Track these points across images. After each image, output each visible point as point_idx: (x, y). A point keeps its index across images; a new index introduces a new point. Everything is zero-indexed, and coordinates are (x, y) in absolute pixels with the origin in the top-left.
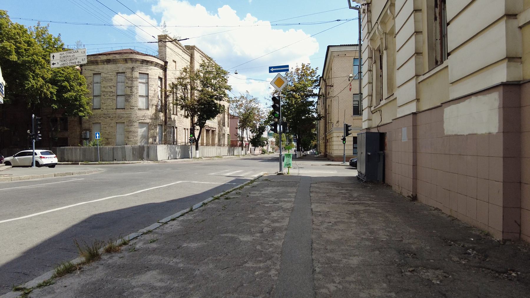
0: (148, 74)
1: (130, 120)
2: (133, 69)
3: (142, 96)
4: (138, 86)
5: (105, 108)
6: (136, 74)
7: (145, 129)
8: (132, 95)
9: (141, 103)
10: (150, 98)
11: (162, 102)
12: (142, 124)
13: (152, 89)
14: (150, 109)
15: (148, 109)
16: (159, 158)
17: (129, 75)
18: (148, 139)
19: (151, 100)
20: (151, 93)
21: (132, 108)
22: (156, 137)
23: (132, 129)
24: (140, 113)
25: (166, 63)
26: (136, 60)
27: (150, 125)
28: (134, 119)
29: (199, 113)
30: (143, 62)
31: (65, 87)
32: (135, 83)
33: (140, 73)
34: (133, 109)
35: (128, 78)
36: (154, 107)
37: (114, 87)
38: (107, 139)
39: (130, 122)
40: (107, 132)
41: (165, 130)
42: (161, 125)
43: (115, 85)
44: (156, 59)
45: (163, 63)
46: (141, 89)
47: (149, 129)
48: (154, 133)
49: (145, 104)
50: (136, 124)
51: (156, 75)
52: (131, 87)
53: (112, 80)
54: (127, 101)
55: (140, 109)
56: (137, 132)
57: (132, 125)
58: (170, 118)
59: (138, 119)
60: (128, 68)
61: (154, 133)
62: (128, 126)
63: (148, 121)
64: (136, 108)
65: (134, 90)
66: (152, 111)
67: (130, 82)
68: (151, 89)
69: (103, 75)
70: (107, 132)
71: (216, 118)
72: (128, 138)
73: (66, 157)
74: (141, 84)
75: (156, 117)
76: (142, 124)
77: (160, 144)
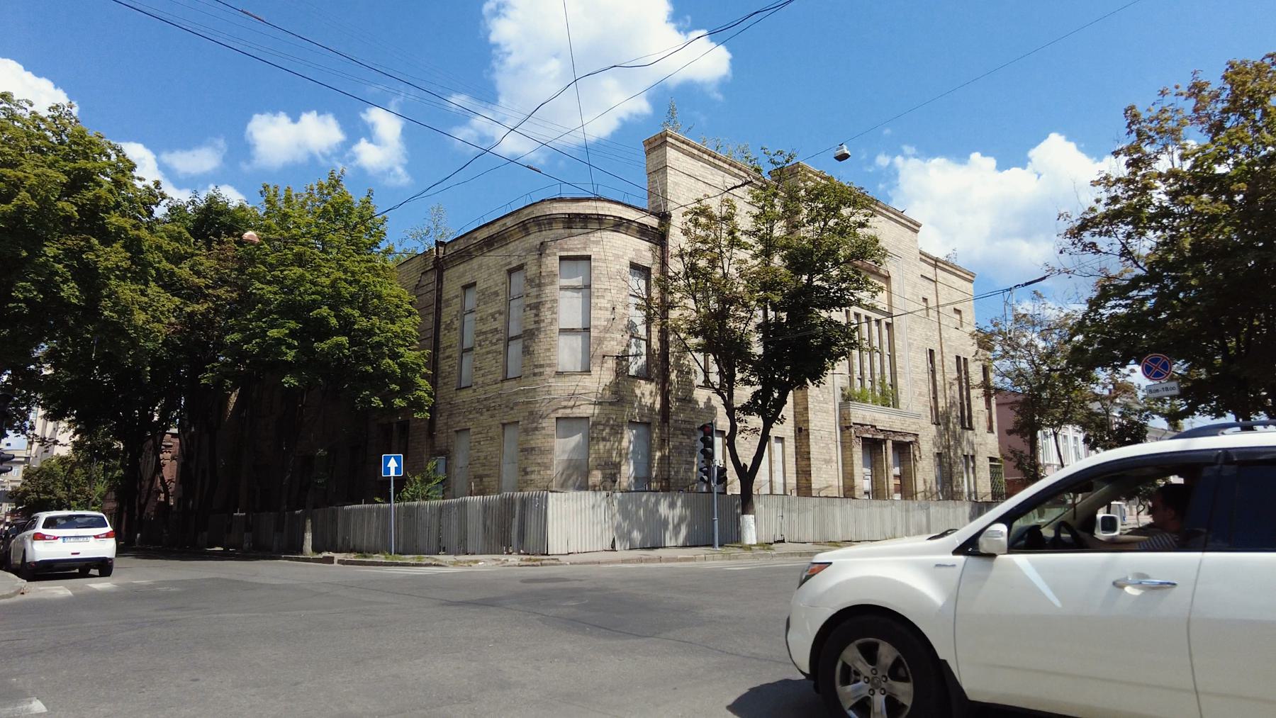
0: (588, 258)
1: (531, 413)
2: (542, 249)
3: (571, 331)
4: (555, 301)
5: (480, 381)
6: (552, 263)
7: (577, 438)
8: (538, 329)
9: (566, 353)
10: (594, 333)
11: (649, 346)
12: (568, 423)
13: (603, 303)
14: (595, 370)
15: (587, 371)
16: (556, 544)
17: (532, 270)
18: (587, 474)
19: (600, 341)
20: (600, 318)
21: (536, 371)
22: (617, 466)
23: (537, 441)
24: (560, 387)
25: (665, 217)
26: (550, 220)
27: (595, 424)
28: (544, 409)
29: (788, 368)
30: (572, 221)
31: (322, 320)
32: (548, 290)
33: (562, 258)
34: (541, 374)
35: (530, 281)
36: (611, 363)
37: (500, 313)
38: (481, 477)
39: (535, 417)
40: (482, 455)
41: (663, 442)
42: (648, 424)
43: (503, 309)
44: (620, 207)
45: (653, 222)
46: (568, 310)
47: (590, 440)
48: (609, 452)
49: (580, 356)
50: (549, 424)
51: (617, 257)
52: (537, 307)
53: (496, 294)
54: (527, 351)
55: (559, 374)
56: (551, 451)
57: (536, 429)
58: (688, 400)
59: (554, 405)
60: (529, 251)
61: (609, 452)
62: (526, 431)
63: (587, 410)
64: (548, 370)
65: (546, 314)
66: (603, 376)
67: (534, 291)
68: (601, 304)
69: (481, 285)
70: (482, 455)
71: (828, 378)
72: (527, 473)
73: (340, 541)
74: (569, 293)
75: (619, 394)
76: (568, 423)
77: (563, 486)
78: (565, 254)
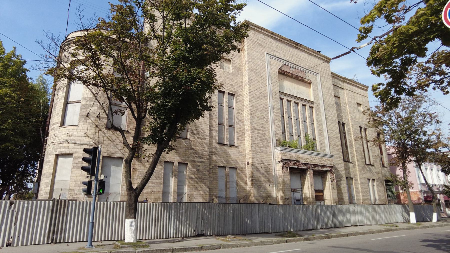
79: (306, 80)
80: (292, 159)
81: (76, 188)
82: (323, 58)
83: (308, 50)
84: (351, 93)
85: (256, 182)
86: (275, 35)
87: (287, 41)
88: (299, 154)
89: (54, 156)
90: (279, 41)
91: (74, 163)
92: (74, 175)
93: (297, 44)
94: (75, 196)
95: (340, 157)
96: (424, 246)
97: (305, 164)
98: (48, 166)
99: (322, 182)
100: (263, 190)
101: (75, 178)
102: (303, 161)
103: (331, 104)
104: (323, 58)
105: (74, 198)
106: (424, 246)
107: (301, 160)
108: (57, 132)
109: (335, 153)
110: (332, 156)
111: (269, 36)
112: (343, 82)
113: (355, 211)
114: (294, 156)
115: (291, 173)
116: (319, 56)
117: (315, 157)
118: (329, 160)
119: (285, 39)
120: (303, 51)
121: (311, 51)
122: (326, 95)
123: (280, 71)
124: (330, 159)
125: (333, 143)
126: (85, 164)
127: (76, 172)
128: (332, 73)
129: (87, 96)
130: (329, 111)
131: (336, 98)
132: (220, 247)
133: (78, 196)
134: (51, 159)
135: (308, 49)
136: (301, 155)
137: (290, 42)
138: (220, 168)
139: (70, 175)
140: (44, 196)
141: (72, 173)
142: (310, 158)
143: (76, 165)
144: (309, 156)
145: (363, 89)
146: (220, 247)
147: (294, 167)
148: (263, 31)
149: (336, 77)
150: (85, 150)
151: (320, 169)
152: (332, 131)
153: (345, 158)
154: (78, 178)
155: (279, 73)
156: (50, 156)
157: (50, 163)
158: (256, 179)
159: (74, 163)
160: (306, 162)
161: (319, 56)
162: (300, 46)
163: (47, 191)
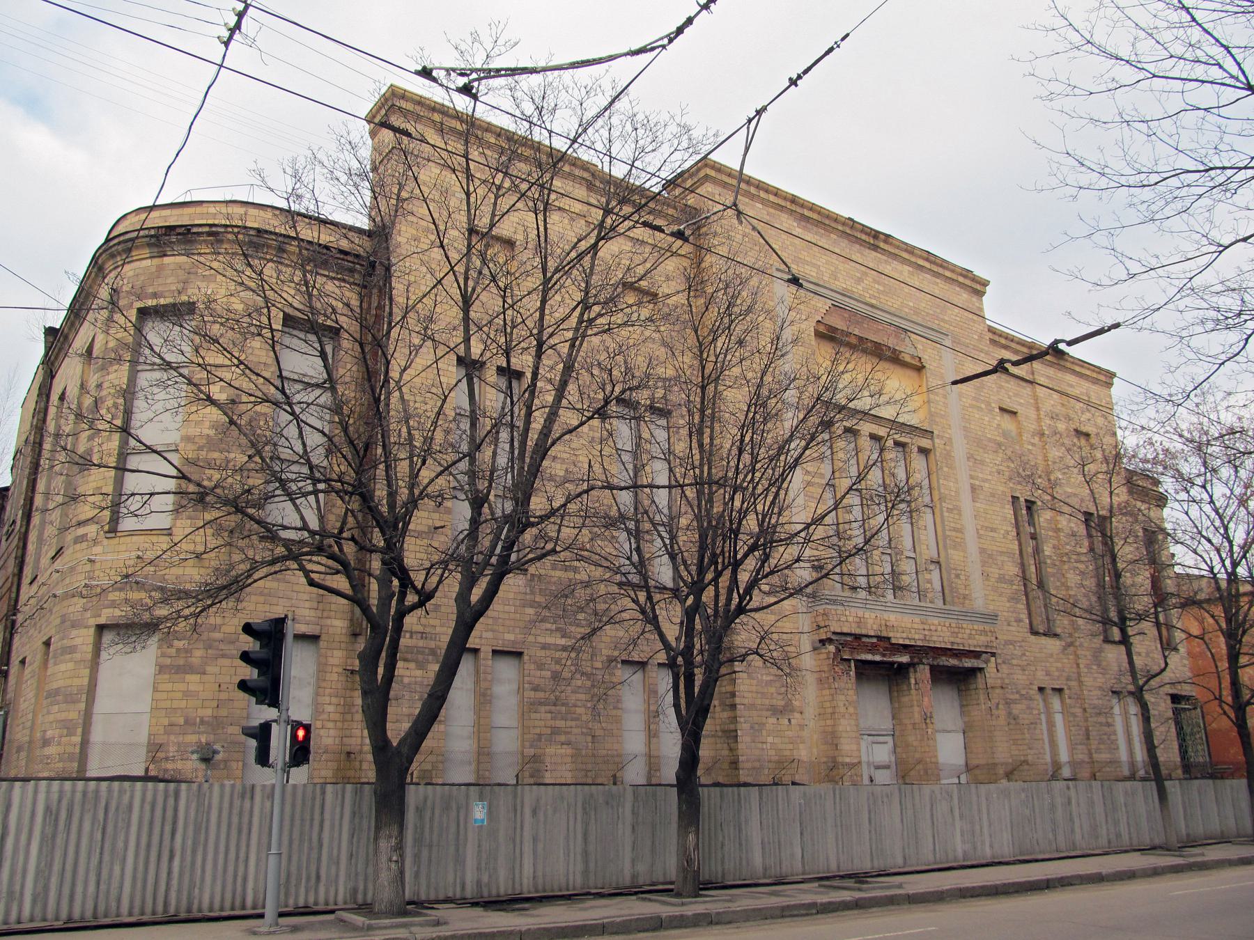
78: (150, 303)
79: (908, 359)
80: (864, 632)
81: (172, 737)
82: (961, 279)
83: (911, 253)
84: (1056, 396)
85: (746, 713)
86: (802, 206)
87: (844, 224)
88: (886, 616)
89: (92, 631)
90: (818, 224)
91: (163, 655)
92: (164, 696)
93: (876, 234)
94: (170, 766)
95: (1019, 621)
96: (93, 340)
97: (906, 648)
98: (71, 665)
99: (962, 706)
100: (770, 739)
101: (168, 704)
102: (898, 638)
103: (990, 440)
104: (961, 279)
105: (166, 770)
106: (93, 340)
107: (891, 635)
108: (97, 549)
109: (1001, 605)
110: (993, 617)
111: (781, 208)
112: (1172, 867)
113: (1069, 802)
114: (870, 621)
115: (860, 676)
116: (948, 274)
117: (936, 621)
118: (984, 632)
119: (836, 220)
120: (895, 256)
121: (921, 257)
122: (972, 406)
123: (822, 329)
124: (987, 628)
125: (995, 572)
126: (250, 673)
127: (169, 686)
128: (991, 330)
129: (197, 431)
130: (982, 462)
131: (1006, 416)
132: (658, 924)
133: (179, 765)
134: (78, 641)
135: (910, 249)
136: (892, 618)
137: (852, 227)
138: (625, 667)
139: (148, 696)
140: (60, 765)
141: (155, 690)
142: (921, 627)
143: (168, 661)
144: (917, 620)
145: (1095, 381)
146: (658, 924)
147: (869, 657)
148: (762, 194)
149: (1003, 341)
150: (248, 629)
151: (953, 662)
152: (993, 530)
153: (1035, 624)
154: (176, 704)
155: (818, 335)
156: (74, 633)
157: (77, 656)
158: (746, 701)
159: (163, 655)
160: (907, 642)
161: (948, 274)
162: (886, 242)
163: (70, 749)
